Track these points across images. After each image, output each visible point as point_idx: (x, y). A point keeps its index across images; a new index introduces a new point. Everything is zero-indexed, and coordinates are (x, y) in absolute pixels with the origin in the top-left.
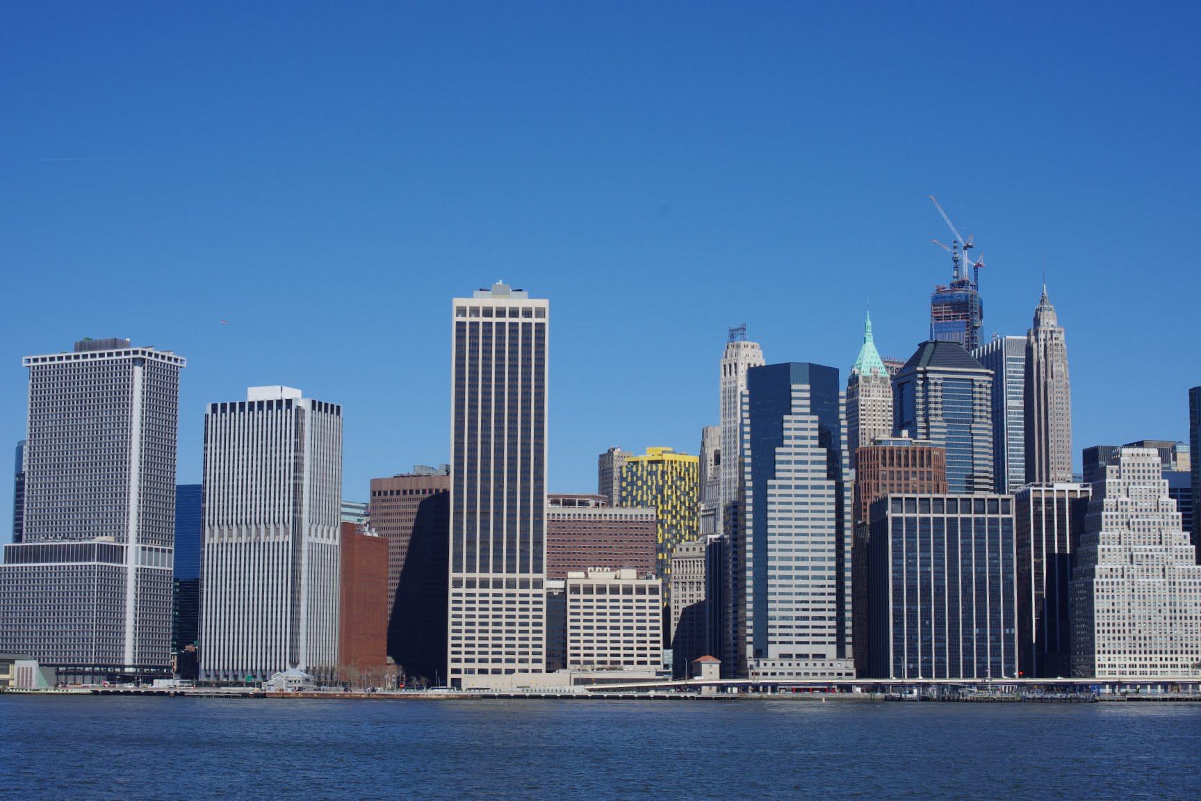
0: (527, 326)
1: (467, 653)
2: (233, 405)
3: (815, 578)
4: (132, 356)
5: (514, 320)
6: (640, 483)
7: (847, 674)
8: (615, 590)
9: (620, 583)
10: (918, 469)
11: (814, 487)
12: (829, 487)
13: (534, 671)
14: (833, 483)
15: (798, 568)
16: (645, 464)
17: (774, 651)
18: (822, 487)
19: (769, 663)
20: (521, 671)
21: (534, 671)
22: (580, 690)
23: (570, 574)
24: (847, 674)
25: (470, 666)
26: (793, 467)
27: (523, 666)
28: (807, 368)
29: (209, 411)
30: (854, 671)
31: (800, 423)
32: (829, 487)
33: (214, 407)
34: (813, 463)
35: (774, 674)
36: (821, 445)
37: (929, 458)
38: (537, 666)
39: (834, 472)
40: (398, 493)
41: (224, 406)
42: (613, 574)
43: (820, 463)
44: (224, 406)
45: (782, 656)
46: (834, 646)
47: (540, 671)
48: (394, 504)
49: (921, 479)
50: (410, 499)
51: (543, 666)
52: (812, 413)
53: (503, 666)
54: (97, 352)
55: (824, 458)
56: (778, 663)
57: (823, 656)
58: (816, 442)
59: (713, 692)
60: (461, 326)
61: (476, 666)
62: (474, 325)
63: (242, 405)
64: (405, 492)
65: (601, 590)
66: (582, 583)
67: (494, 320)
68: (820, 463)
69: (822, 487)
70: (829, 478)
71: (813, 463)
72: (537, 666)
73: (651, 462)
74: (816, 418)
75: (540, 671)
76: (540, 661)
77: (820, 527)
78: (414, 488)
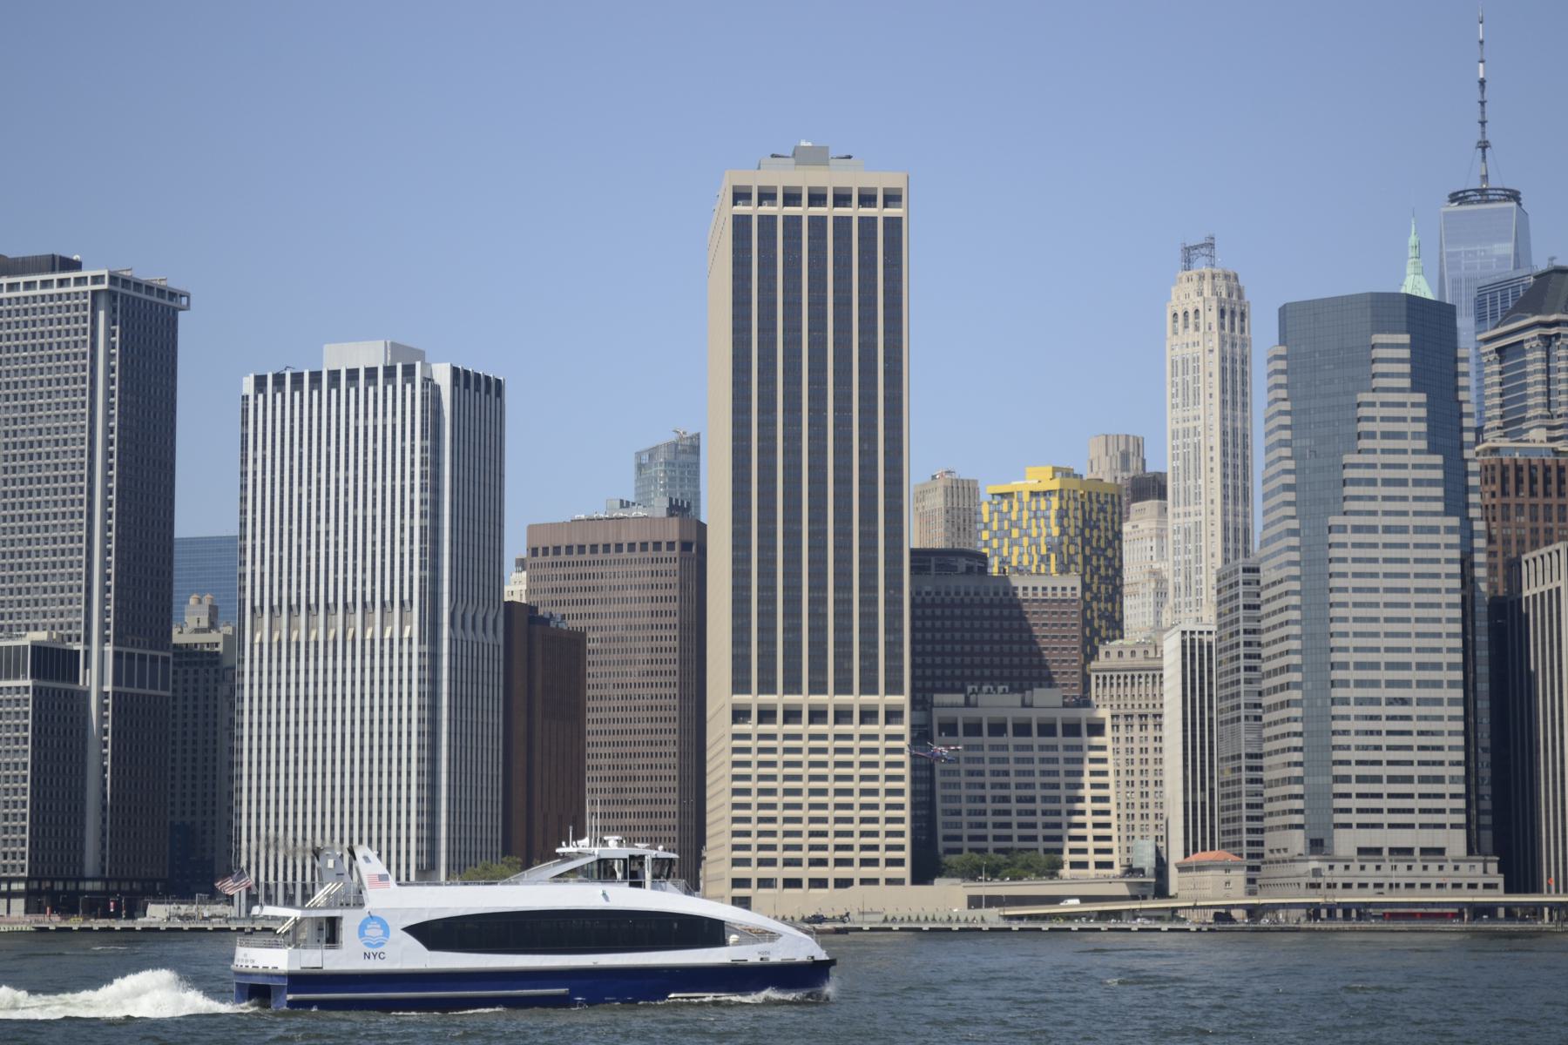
0: (868, 224)
1: (864, 848)
2: (297, 379)
3: (1360, 702)
4: (89, 287)
5: (842, 211)
6: (1015, 533)
7: (1486, 886)
8: (1022, 729)
9: (1034, 716)
10: (1540, 500)
11: (1419, 530)
12: (1450, 530)
13: (889, 881)
14: (1454, 521)
15: (1360, 684)
16: (1026, 497)
17: (1346, 843)
18: (1434, 530)
19: (1449, 867)
20: (863, 881)
21: (889, 881)
22: (992, 917)
23: (938, 698)
24: (1486, 886)
25: (766, 872)
26: (1381, 491)
27: (869, 872)
28: (1404, 305)
29: (248, 386)
30: (1500, 880)
31: (1393, 404)
32: (1450, 530)
33: (260, 382)
34: (1418, 483)
35: (1347, 886)
36: (1432, 450)
37: (1504, 480)
38: (895, 872)
39: (1456, 501)
40: (619, 547)
41: (279, 380)
42: (1016, 699)
43: (1431, 483)
44: (279, 380)
45: (1361, 851)
46: (1462, 833)
47: (900, 882)
48: (573, 570)
49: (1534, 518)
50: (642, 561)
51: (904, 872)
52: (1414, 389)
53: (831, 872)
54: (22, 279)
55: (1438, 474)
56: (1355, 866)
57: (1441, 851)
58: (1422, 444)
59: (1296, 917)
60: (741, 223)
61: (779, 872)
62: (767, 222)
63: (316, 377)
64: (619, 547)
65: (998, 729)
66: (962, 715)
67: (804, 211)
68: (1431, 483)
69: (1434, 530)
70: (1447, 512)
71: (1418, 483)
72: (895, 872)
73: (1033, 494)
74: (1421, 397)
75: (900, 882)
76: (899, 862)
77: (1432, 605)
78: (612, 541)
